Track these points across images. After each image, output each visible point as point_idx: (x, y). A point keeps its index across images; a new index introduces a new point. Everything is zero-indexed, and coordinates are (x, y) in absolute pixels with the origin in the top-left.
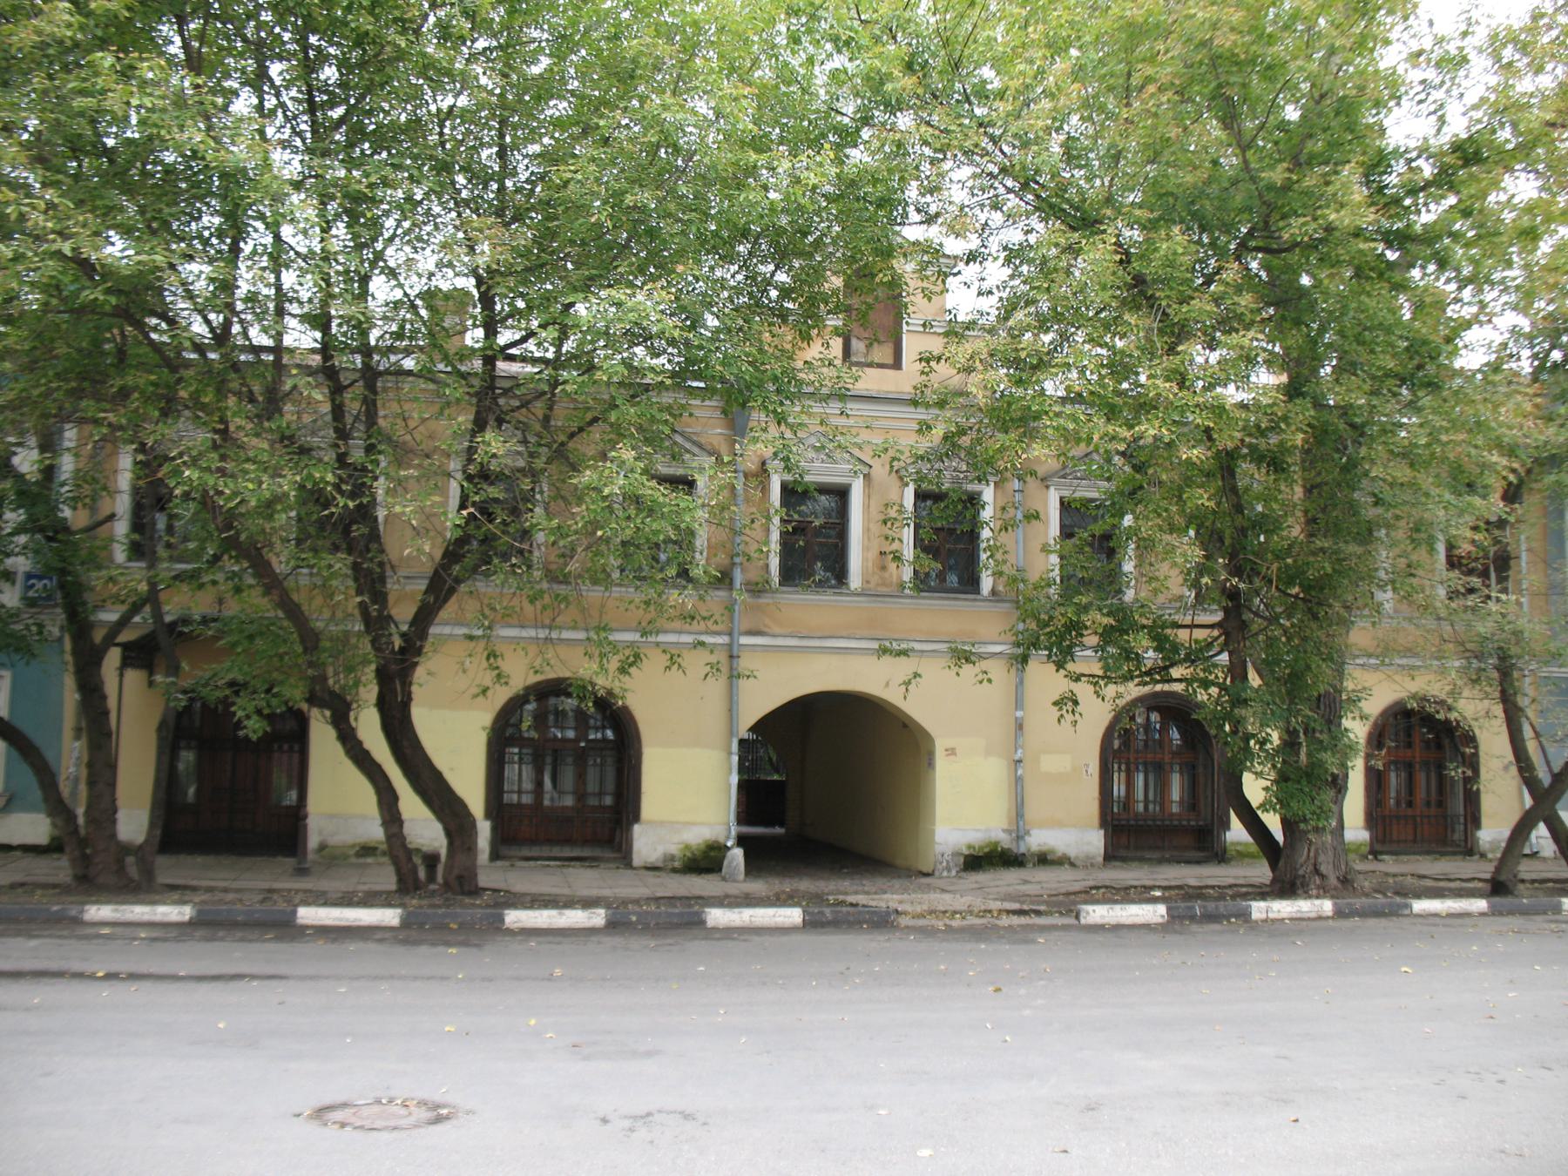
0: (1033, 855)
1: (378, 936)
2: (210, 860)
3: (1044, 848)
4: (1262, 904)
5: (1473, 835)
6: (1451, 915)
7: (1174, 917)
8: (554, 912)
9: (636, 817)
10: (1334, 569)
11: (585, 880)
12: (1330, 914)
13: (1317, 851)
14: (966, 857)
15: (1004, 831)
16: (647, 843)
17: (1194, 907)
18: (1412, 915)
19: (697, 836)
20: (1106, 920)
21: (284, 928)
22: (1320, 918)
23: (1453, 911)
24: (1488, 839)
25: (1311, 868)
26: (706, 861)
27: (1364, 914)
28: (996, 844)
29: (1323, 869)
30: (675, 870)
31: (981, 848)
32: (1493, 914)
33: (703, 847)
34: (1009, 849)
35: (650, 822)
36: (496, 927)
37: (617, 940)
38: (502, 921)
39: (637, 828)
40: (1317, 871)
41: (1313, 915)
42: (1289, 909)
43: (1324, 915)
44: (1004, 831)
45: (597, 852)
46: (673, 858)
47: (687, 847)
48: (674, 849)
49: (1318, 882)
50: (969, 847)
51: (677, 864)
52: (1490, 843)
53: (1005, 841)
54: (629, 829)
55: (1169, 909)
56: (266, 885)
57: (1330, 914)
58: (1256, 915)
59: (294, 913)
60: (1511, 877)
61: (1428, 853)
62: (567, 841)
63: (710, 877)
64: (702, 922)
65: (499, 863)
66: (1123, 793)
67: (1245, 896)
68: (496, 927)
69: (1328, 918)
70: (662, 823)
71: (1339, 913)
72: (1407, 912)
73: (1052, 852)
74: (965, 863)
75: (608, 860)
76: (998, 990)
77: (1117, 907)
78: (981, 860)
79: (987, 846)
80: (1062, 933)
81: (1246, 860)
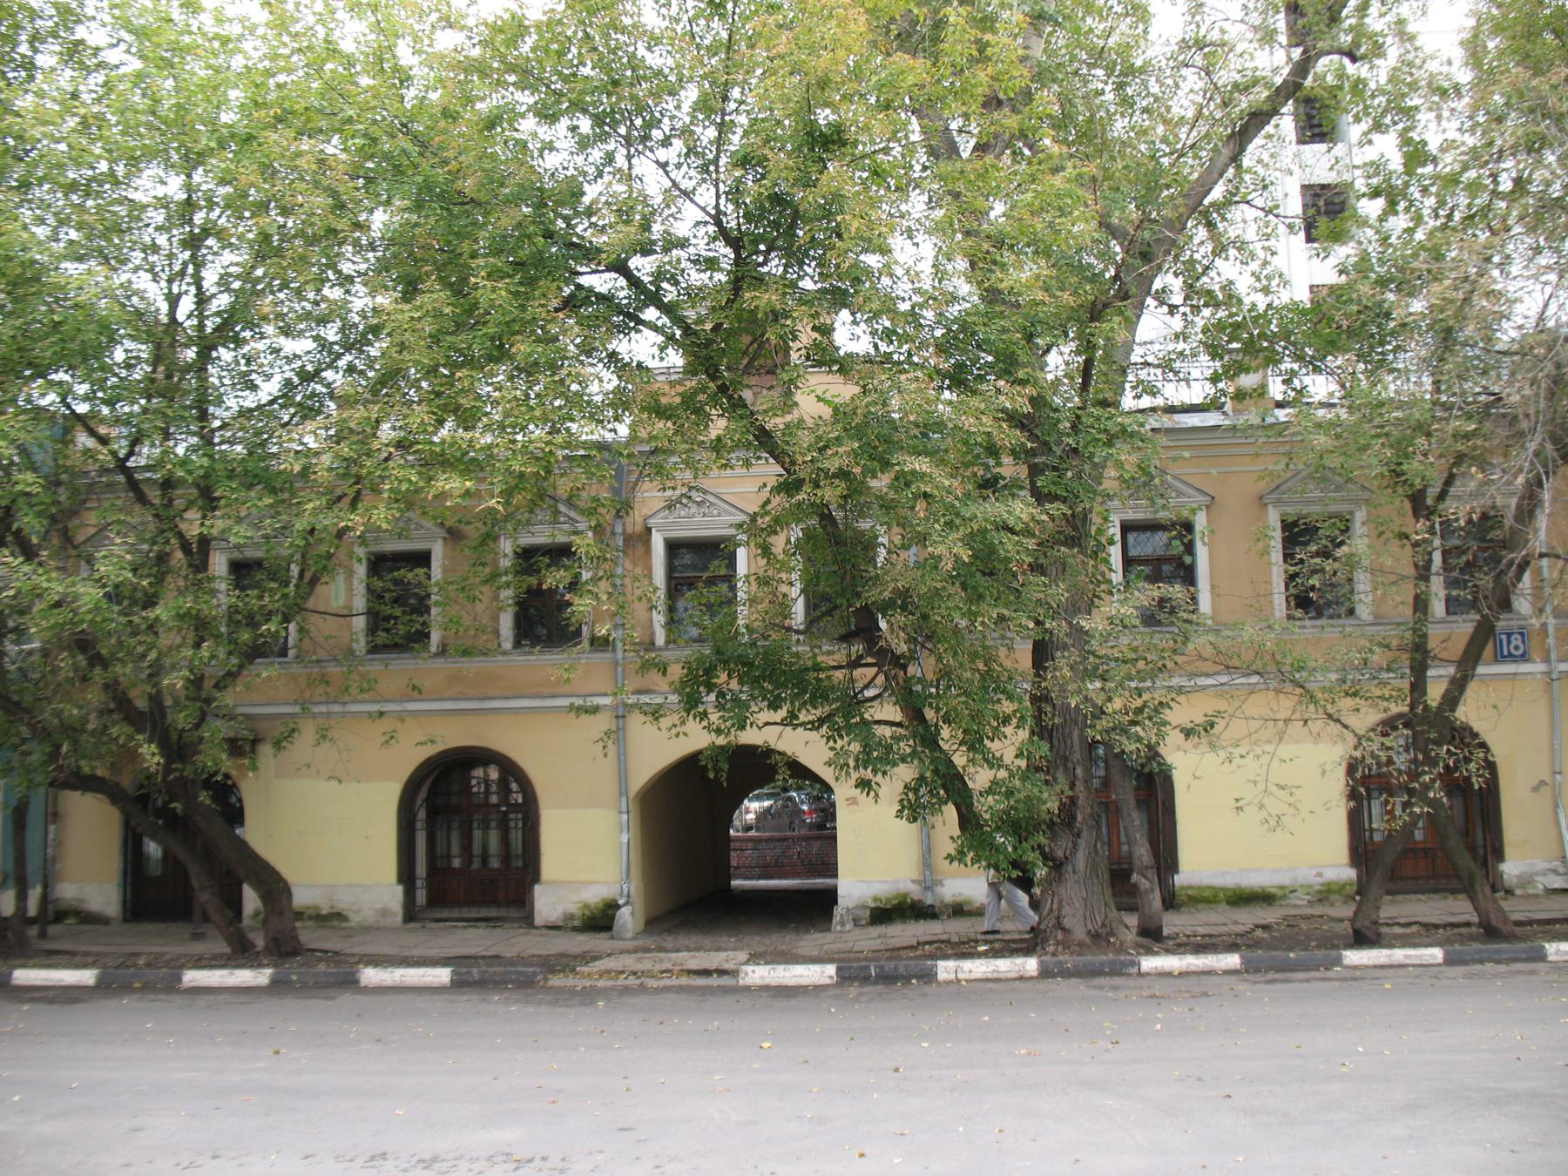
0: (947, 906)
1: (29, 996)
2: (161, 926)
3: (959, 899)
4: (951, 964)
5: (1495, 869)
6: (1182, 974)
7: (460, 984)
8: (225, 972)
9: (536, 877)
10: (325, 299)
11: (811, 941)
12: (1035, 974)
13: (1060, 902)
14: (873, 910)
15: (913, 881)
16: (549, 903)
17: (868, 967)
18: (1140, 974)
19: (594, 895)
20: (766, 982)
21: (171, 986)
22: (1021, 978)
23: (1193, 968)
24: (1515, 872)
25: (1053, 921)
26: (600, 920)
27: (1066, 974)
28: (905, 895)
29: (1067, 923)
30: (575, 929)
31: (888, 900)
32: (1247, 971)
33: (601, 906)
34: (920, 901)
35: (551, 883)
36: (349, 982)
37: (292, 1004)
38: (180, 980)
39: (537, 888)
40: (1059, 925)
41: (1013, 975)
42: (983, 969)
43: (1028, 975)
44: (913, 881)
45: (503, 912)
46: (572, 917)
47: (586, 906)
48: (573, 908)
49: (1060, 937)
50: (875, 899)
51: (576, 923)
52: (1518, 877)
53: (915, 892)
54: (531, 891)
55: (839, 970)
56: (130, 949)
57: (1035, 974)
58: (942, 976)
59: (10, 974)
60: (1367, 923)
61: (1435, 891)
62: (493, 902)
63: (603, 935)
64: (357, 982)
65: (412, 925)
66: (477, 834)
67: (935, 957)
68: (349, 982)
69: (1032, 978)
70: (562, 883)
71: (1045, 973)
72: (1134, 970)
73: (969, 902)
74: (872, 916)
75: (511, 920)
76: (277, 1052)
77: (781, 968)
78: (885, 913)
79: (896, 897)
80: (675, 996)
81: (1200, 906)
